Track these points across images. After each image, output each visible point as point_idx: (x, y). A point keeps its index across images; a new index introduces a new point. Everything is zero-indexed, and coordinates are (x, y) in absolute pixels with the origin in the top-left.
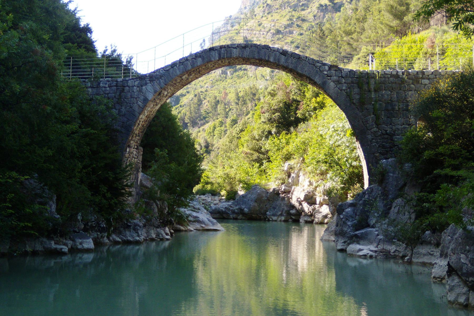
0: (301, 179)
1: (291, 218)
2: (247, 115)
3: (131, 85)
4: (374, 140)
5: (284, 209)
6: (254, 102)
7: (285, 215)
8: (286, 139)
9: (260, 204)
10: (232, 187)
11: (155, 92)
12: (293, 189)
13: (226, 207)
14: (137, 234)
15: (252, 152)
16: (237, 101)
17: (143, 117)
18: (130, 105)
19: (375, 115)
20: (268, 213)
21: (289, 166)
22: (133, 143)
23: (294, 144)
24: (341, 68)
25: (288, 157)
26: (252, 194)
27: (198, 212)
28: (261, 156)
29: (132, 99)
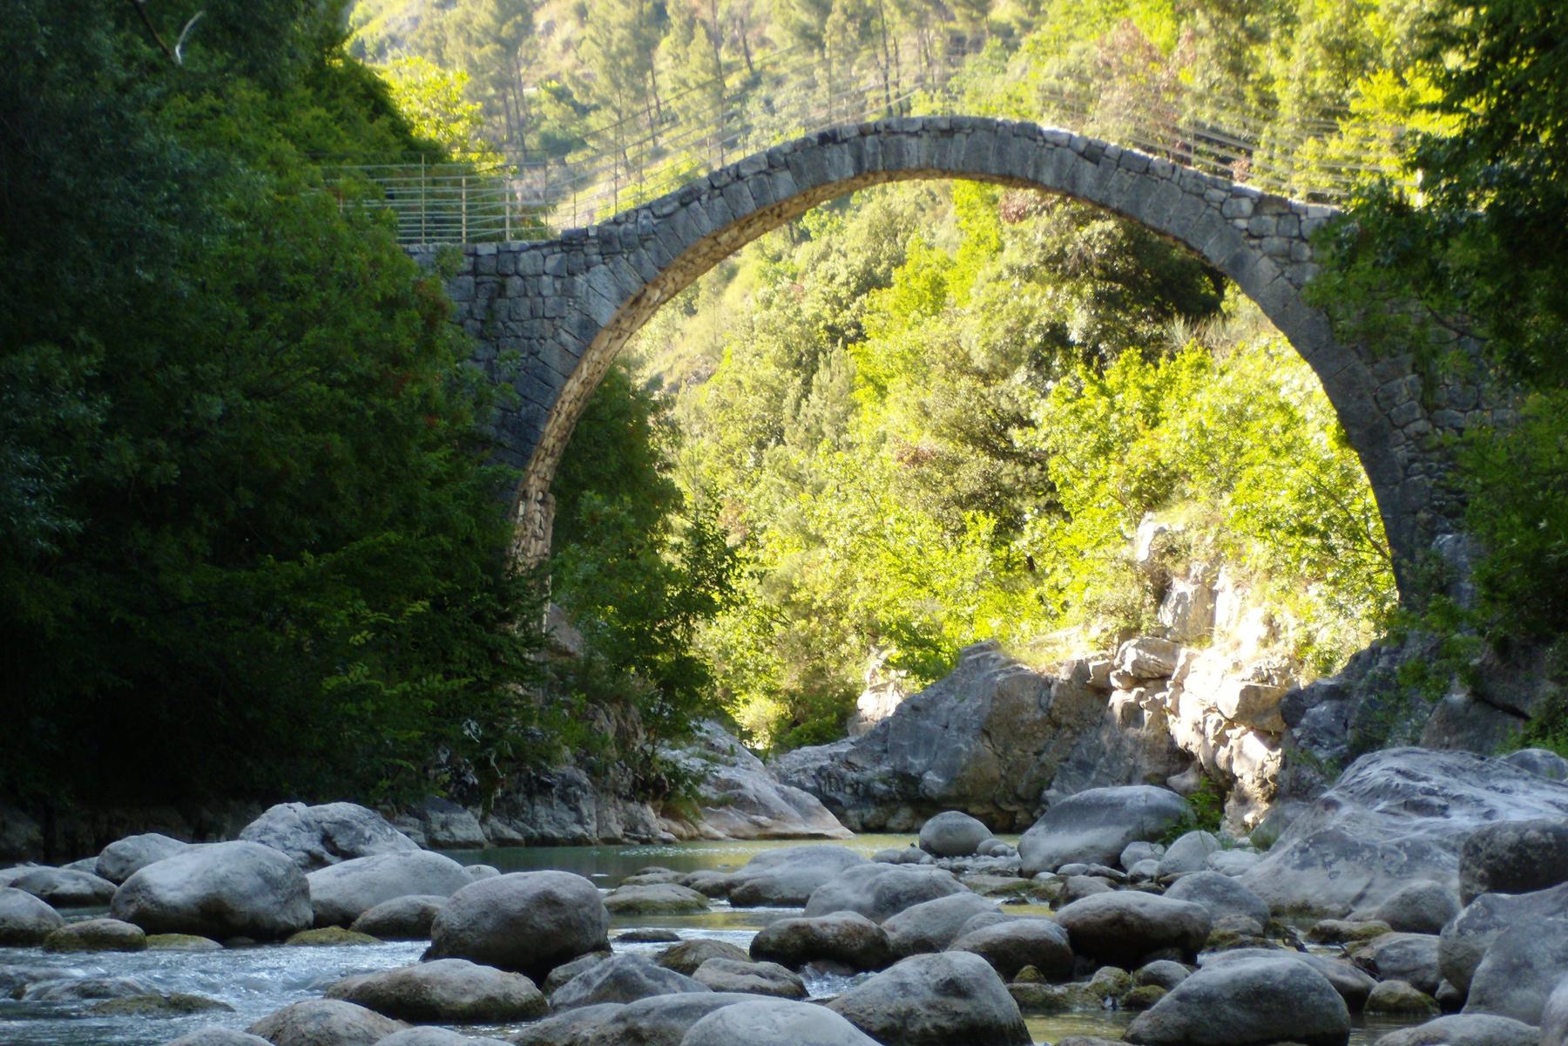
0: (1225, 605)
3: (529, 271)
4: (1416, 465)
8: (1147, 389)
9: (1007, 748)
10: (820, 672)
11: (623, 296)
12: (1181, 661)
14: (573, 815)
15: (946, 447)
16: (808, 18)
17: (573, 387)
18: (531, 346)
19: (1421, 375)
20: (1051, 793)
21: (1161, 539)
22: (535, 485)
23: (1184, 423)
24: (1298, 207)
26: (966, 691)
27: (734, 765)
28: (1009, 472)
29: (537, 323)
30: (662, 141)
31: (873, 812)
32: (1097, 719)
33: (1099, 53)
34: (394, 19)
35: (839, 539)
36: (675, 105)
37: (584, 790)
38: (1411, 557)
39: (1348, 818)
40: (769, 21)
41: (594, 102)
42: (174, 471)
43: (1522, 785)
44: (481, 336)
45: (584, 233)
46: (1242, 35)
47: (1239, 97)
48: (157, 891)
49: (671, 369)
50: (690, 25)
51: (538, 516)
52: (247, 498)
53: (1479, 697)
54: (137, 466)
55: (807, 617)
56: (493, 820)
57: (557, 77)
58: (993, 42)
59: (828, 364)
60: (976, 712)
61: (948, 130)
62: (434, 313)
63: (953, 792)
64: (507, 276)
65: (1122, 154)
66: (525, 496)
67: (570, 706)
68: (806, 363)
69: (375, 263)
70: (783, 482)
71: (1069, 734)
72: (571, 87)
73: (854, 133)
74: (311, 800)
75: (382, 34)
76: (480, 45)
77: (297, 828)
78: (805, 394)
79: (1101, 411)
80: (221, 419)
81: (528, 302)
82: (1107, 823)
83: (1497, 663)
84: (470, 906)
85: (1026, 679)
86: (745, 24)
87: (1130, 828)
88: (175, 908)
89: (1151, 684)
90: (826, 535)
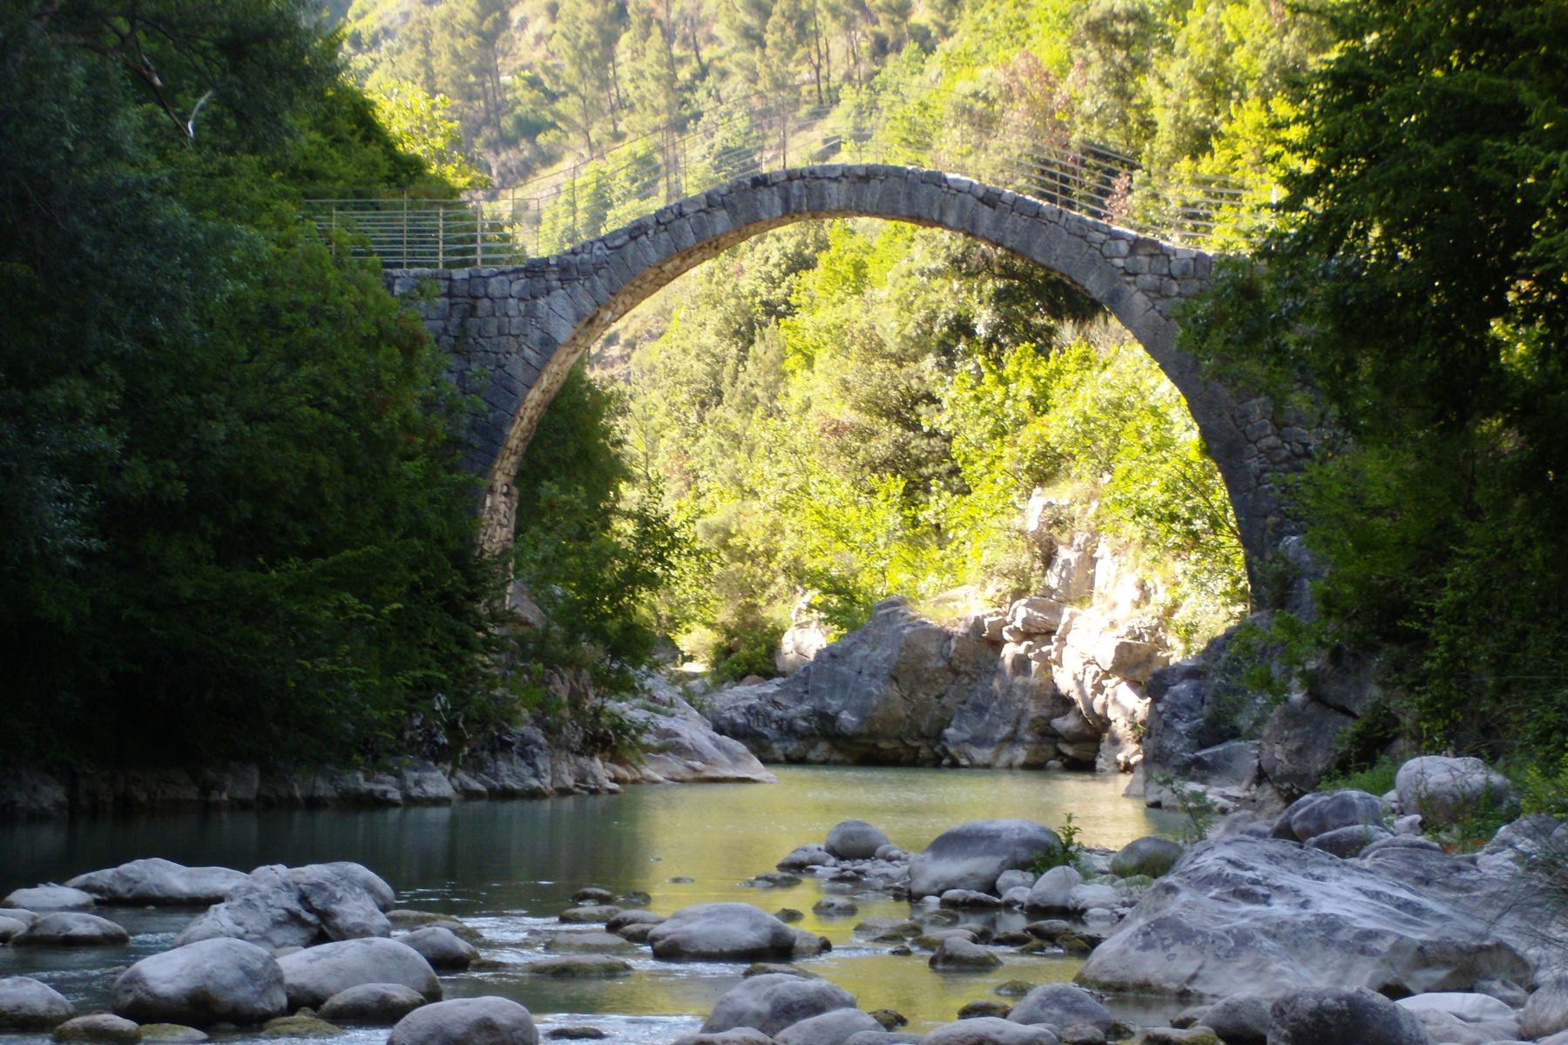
0: (1104, 570)
1: (1059, 754)
2: (819, 114)
3: (497, 294)
5: (1023, 712)
6: (869, 29)
7: (1028, 737)
9: (912, 692)
11: (579, 318)
12: (1065, 619)
13: (750, 708)
14: (531, 770)
15: (864, 420)
17: (534, 395)
20: (950, 732)
21: (1049, 512)
22: (500, 480)
25: (1047, 467)
26: (878, 640)
29: (503, 340)
30: (622, 127)
31: (795, 745)
32: (991, 668)
33: (1001, 77)
34: (387, 14)
35: (772, 494)
36: (634, 95)
37: (540, 748)
38: (1262, 558)
39: (1184, 905)
40: (715, 21)
41: (563, 89)
42: (182, 489)
43: (1334, 872)
44: (455, 351)
45: (545, 261)
46: (1128, 65)
47: (1124, 120)
48: (152, 984)
49: (626, 327)
50: (647, 23)
51: (503, 507)
52: (246, 509)
53: (1315, 696)
54: (150, 484)
55: (741, 559)
56: (461, 774)
57: (530, 67)
58: (911, 47)
59: (763, 338)
60: (886, 660)
61: (867, 176)
62: (410, 345)
63: (864, 729)
64: (477, 298)
65: (1016, 200)
66: (491, 490)
67: (529, 673)
68: (745, 333)
69: (360, 306)
70: (722, 441)
71: (966, 680)
72: (543, 76)
73: (783, 178)
74: (291, 864)
75: (377, 26)
76: (463, 36)
77: (277, 889)
78: (742, 360)
79: (998, 399)
80: (224, 443)
81: (495, 322)
82: (985, 853)
83: (1330, 668)
84: (419, 1029)
85: (926, 631)
86: (695, 22)
87: (1005, 857)
88: (167, 999)
89: (1038, 638)
90: (758, 489)
